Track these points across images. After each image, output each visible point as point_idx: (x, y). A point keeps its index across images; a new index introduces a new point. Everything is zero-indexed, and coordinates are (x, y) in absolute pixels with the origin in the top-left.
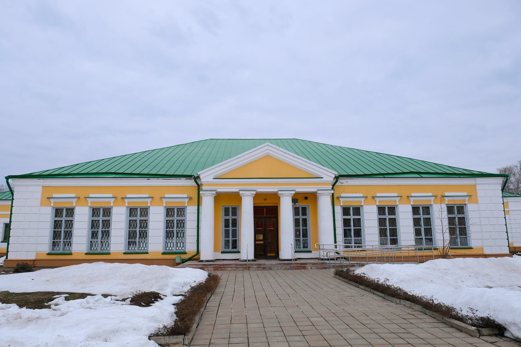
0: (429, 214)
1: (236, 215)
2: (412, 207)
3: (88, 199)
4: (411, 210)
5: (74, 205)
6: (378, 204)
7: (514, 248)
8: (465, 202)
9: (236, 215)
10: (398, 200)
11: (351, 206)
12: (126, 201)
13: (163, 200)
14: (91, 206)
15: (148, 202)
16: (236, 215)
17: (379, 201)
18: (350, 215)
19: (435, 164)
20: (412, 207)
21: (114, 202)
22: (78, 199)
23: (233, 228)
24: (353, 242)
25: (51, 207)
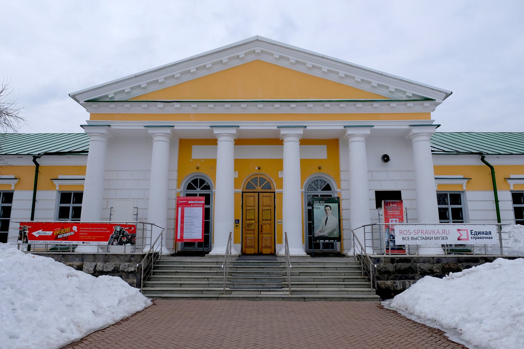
0: (61, 209)
1: (209, 204)
2: (512, 193)
3: (55, 182)
4: (510, 197)
5: (13, 188)
6: (512, 188)
7: (345, 281)
8: (462, 188)
9: (209, 204)
10: (465, 184)
11: (448, 192)
12: (56, 184)
13: (54, 183)
14: (60, 190)
15: (11, 185)
16: (209, 204)
17: (514, 185)
18: (74, 208)
19: (450, 133)
20: (512, 193)
21: (16, 185)
22: (468, 181)
23: (209, 220)
24: (390, 252)
25: (56, 191)
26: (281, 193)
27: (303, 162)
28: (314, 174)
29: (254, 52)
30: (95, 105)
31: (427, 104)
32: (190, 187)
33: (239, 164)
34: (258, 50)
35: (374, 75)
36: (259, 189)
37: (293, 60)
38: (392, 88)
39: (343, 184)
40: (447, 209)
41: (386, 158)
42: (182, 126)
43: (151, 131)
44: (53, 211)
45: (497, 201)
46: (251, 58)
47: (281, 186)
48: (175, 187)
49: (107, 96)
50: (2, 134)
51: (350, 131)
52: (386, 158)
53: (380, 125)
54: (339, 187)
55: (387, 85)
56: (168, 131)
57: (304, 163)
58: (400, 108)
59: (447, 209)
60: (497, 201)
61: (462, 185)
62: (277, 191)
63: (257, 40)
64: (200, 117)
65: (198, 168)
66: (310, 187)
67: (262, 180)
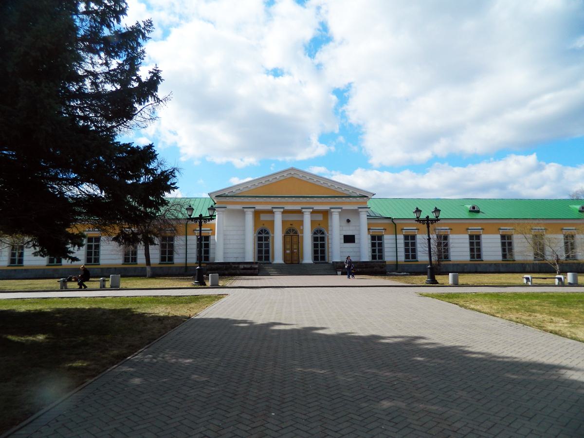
3: (195, 231)
17: (535, 232)
21: (211, 233)
26: (303, 236)
27: (312, 222)
28: (316, 227)
29: (291, 173)
30: (219, 198)
31: (365, 198)
32: (259, 233)
33: (284, 222)
34: (292, 173)
35: (82, 387)
36: (291, 234)
37: (308, 178)
38: (351, 191)
39: (330, 232)
40: (376, 243)
41: (348, 221)
42: (258, 207)
43: (245, 210)
44: (101, 254)
45: (396, 239)
46: (289, 176)
47: (302, 233)
48: (330, 236)
49: (225, 194)
50: (582, 302)
51: (332, 210)
52: (348, 221)
53: (345, 207)
54: (328, 233)
55: (348, 189)
56: (253, 210)
57: (312, 222)
58: (354, 200)
59: (376, 243)
60: (396, 239)
61: (382, 232)
62: (300, 235)
63: (292, 169)
64: (266, 203)
65: (263, 225)
66: (315, 233)
67: (293, 230)
